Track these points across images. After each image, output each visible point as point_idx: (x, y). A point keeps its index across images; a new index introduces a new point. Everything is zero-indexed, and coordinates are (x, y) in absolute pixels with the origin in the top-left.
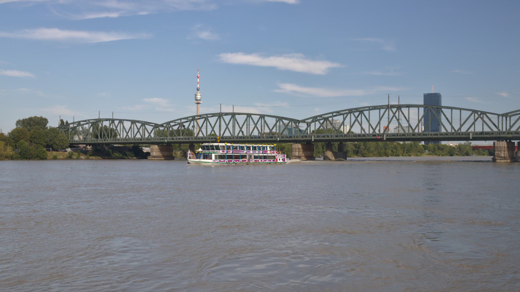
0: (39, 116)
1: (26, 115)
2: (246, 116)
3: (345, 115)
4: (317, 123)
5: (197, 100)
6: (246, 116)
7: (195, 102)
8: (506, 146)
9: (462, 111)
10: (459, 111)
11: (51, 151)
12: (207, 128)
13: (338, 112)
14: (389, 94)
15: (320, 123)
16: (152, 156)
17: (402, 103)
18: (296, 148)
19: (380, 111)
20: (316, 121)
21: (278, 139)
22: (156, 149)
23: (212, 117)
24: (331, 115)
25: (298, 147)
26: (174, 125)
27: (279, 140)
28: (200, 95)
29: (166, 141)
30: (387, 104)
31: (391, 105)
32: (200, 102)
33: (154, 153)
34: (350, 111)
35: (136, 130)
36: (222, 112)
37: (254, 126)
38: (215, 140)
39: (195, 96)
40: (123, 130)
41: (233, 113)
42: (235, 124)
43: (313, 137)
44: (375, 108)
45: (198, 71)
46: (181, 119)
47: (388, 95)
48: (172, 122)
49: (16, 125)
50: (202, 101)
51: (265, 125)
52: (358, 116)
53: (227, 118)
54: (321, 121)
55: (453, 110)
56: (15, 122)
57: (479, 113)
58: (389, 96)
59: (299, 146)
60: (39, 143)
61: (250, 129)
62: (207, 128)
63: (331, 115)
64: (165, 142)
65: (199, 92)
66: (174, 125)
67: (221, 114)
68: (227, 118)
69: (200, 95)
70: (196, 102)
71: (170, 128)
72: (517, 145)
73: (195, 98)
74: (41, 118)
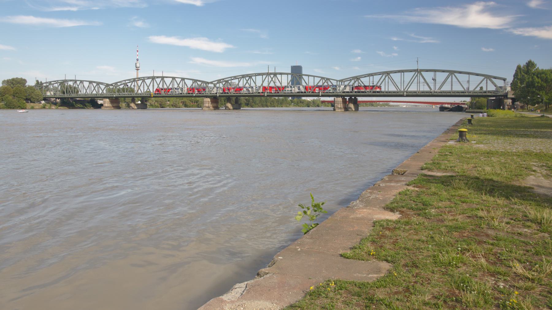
3: (240, 79)
9: (470, 75)
10: (313, 77)
13: (235, 77)
15: (222, 84)
17: (277, 71)
19: (370, 78)
21: (194, 95)
26: (121, 85)
30: (267, 72)
35: (93, 88)
36: (155, 76)
42: (164, 85)
48: (119, 82)
52: (248, 80)
53: (158, 80)
54: (224, 83)
55: (309, 77)
56: (2, 82)
57: (326, 79)
62: (144, 87)
65: (138, 62)
66: (121, 85)
67: (269, 74)
68: (158, 80)
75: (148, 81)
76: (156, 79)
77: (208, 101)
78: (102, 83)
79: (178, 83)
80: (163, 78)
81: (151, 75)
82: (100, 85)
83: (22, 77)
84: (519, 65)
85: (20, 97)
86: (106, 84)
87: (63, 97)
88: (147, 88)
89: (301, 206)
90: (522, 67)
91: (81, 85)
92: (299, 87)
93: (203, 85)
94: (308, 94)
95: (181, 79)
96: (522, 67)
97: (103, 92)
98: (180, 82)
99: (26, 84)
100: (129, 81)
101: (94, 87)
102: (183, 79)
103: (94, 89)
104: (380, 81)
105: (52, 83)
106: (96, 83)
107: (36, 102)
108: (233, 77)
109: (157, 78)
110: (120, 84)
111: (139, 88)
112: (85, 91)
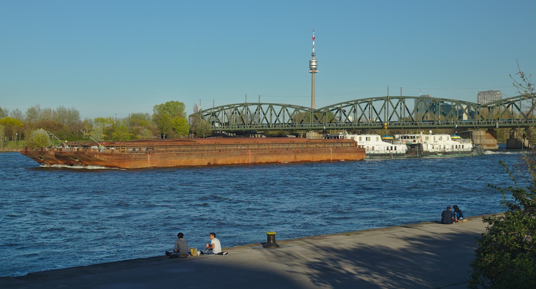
0: (176, 101)
1: (163, 101)
4: (282, 122)
7: (309, 71)
12: (284, 117)
15: (504, 107)
18: (477, 136)
20: (282, 124)
21: (457, 126)
24: (519, 99)
25: (480, 135)
26: (332, 110)
27: (457, 127)
28: (315, 62)
29: (324, 128)
32: (316, 71)
35: (391, 109)
36: (247, 102)
38: (381, 127)
39: (310, 64)
40: (404, 109)
43: (497, 124)
48: (330, 107)
49: (153, 112)
51: (406, 110)
53: (395, 102)
54: (506, 105)
59: (481, 133)
60: (182, 131)
62: (284, 117)
63: (519, 99)
64: (324, 129)
65: (314, 58)
68: (395, 102)
69: (315, 62)
70: (311, 71)
71: (24, 130)
73: (309, 66)
74: (178, 103)
76: (391, 100)
77: (481, 136)
80: (402, 99)
81: (243, 102)
82: (462, 105)
83: (168, 101)
85: (182, 131)
86: (308, 109)
87: (237, 129)
88: (365, 113)
89: (64, 224)
93: (458, 107)
94: (375, 127)
95: (268, 106)
101: (264, 113)
102: (271, 106)
104: (403, 112)
105: (225, 108)
106: (294, 108)
107: (97, 134)
108: (344, 103)
111: (277, 119)
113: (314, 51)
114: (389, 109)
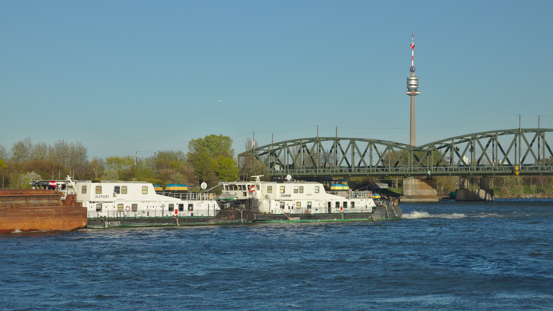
2: (367, 143)
5: (409, 90)
6: (367, 143)
8: (211, 216)
11: (369, 186)
12: (371, 157)
14: (520, 115)
16: (406, 196)
17: (523, 127)
20: (369, 167)
22: (412, 185)
23: (309, 142)
26: (440, 148)
29: (429, 173)
30: (518, 128)
31: (522, 129)
32: (416, 93)
33: (410, 191)
34: (474, 137)
35: (525, 147)
36: (319, 136)
37: (487, 152)
39: (407, 82)
41: (336, 137)
42: (513, 144)
44: (510, 132)
45: (413, 37)
46: (452, 139)
47: (538, 117)
50: (419, 91)
53: (530, 136)
56: (188, 144)
58: (539, 118)
61: (522, 151)
62: (371, 157)
64: (428, 174)
65: (413, 75)
66: (440, 148)
67: (520, 130)
68: (530, 136)
70: (410, 93)
72: (490, 189)
75: (505, 141)
78: (397, 143)
79: (530, 143)
84: (15, 144)
86: (405, 147)
90: (236, 156)
91: (539, 139)
92: (148, 215)
95: (349, 141)
96: (236, 156)
97: (463, 161)
98: (533, 141)
99: (230, 146)
100: (292, 143)
103: (484, 153)
105: (288, 144)
108: (457, 138)
109: (526, 132)
110: (262, 152)
112: (357, 159)
113: (413, 65)
114: (522, 147)
